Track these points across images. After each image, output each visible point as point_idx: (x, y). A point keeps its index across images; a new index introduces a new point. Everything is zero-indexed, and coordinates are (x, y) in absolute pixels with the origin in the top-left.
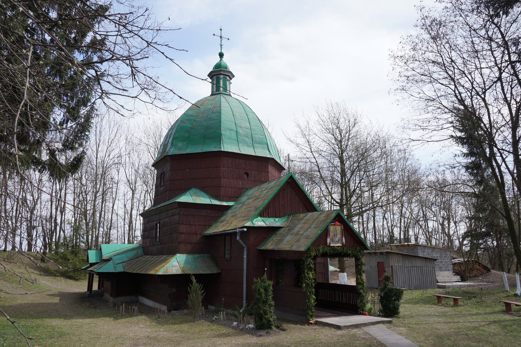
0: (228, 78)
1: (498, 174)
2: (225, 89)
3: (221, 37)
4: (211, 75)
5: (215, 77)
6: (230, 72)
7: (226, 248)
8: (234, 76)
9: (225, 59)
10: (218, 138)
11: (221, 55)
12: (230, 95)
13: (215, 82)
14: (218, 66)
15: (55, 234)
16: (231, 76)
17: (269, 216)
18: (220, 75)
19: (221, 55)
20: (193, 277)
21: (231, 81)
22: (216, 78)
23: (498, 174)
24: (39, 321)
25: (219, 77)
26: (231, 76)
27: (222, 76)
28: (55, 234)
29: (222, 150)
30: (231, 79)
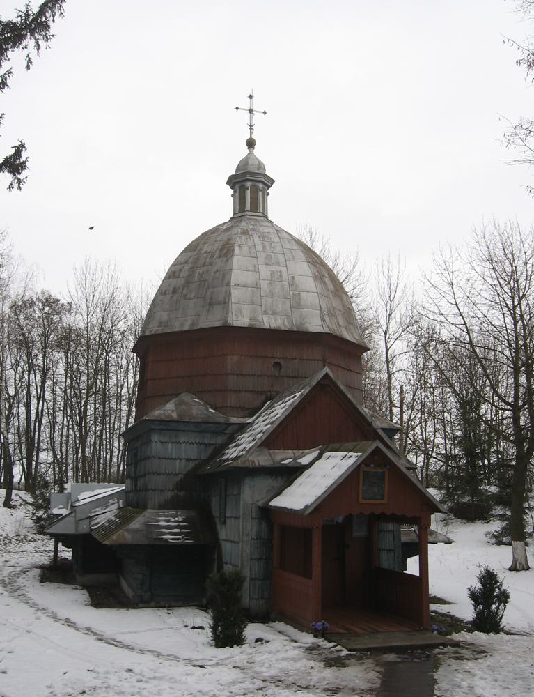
0: (261, 185)
2: (254, 207)
3: (251, 111)
4: (232, 182)
5: (237, 187)
9: (257, 151)
11: (251, 144)
12: (266, 217)
13: (237, 195)
14: (244, 164)
17: (386, 434)
19: (251, 144)
21: (269, 191)
22: (240, 188)
26: (269, 182)
27: (248, 184)
30: (269, 187)
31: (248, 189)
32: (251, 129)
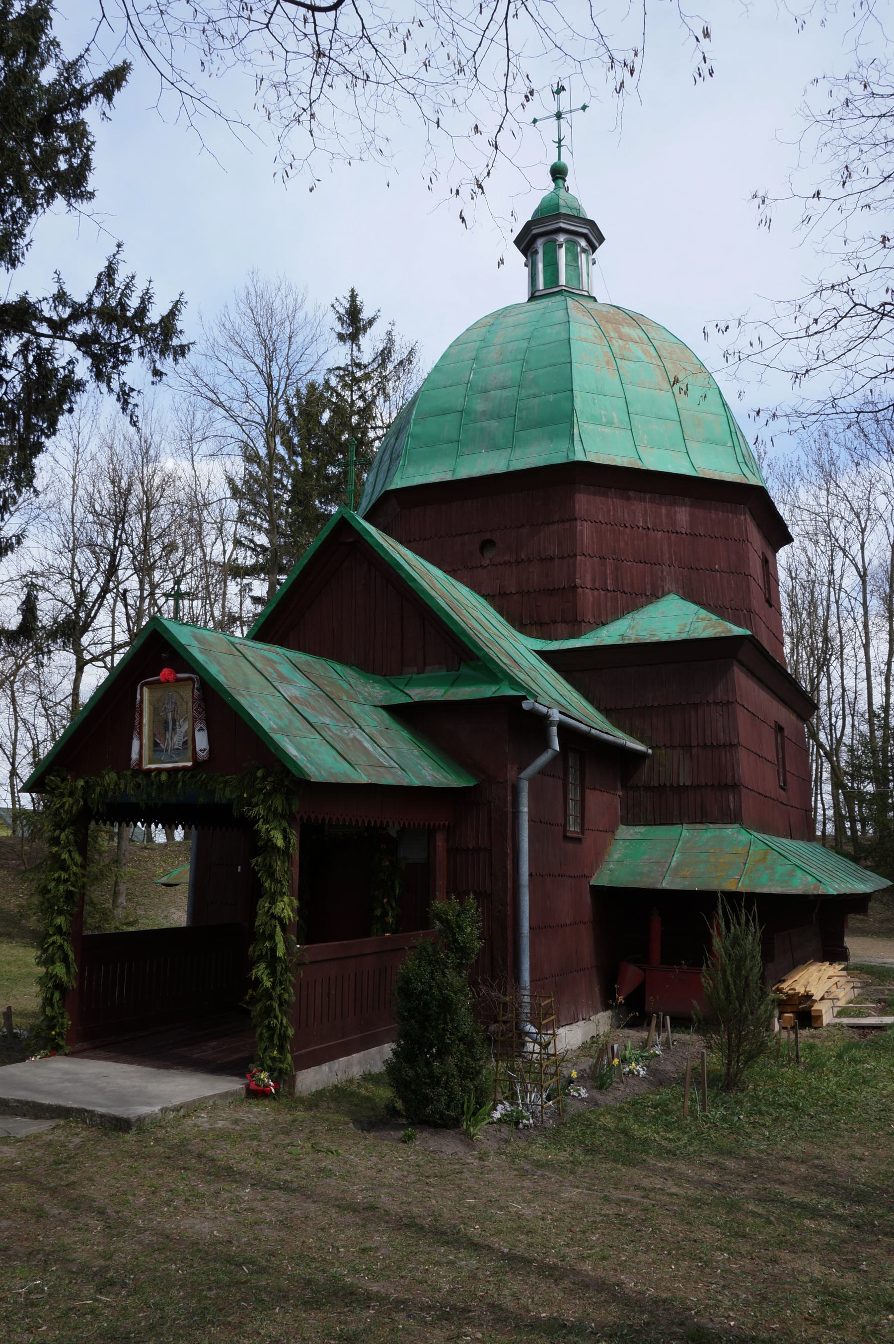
0: (583, 243)
1: (510, 885)
6: (592, 224)
7: (571, 796)
8: (601, 239)
10: (561, 419)
11: (558, 173)
15: (824, 682)
16: (593, 237)
18: (554, 234)
19: (558, 173)
20: (554, 729)
22: (545, 244)
23: (510, 885)
24: (782, 575)
25: (555, 241)
26: (593, 237)
27: (561, 238)
28: (824, 682)
29: (580, 457)
30: (594, 249)
31: (561, 246)
32: (559, 147)
